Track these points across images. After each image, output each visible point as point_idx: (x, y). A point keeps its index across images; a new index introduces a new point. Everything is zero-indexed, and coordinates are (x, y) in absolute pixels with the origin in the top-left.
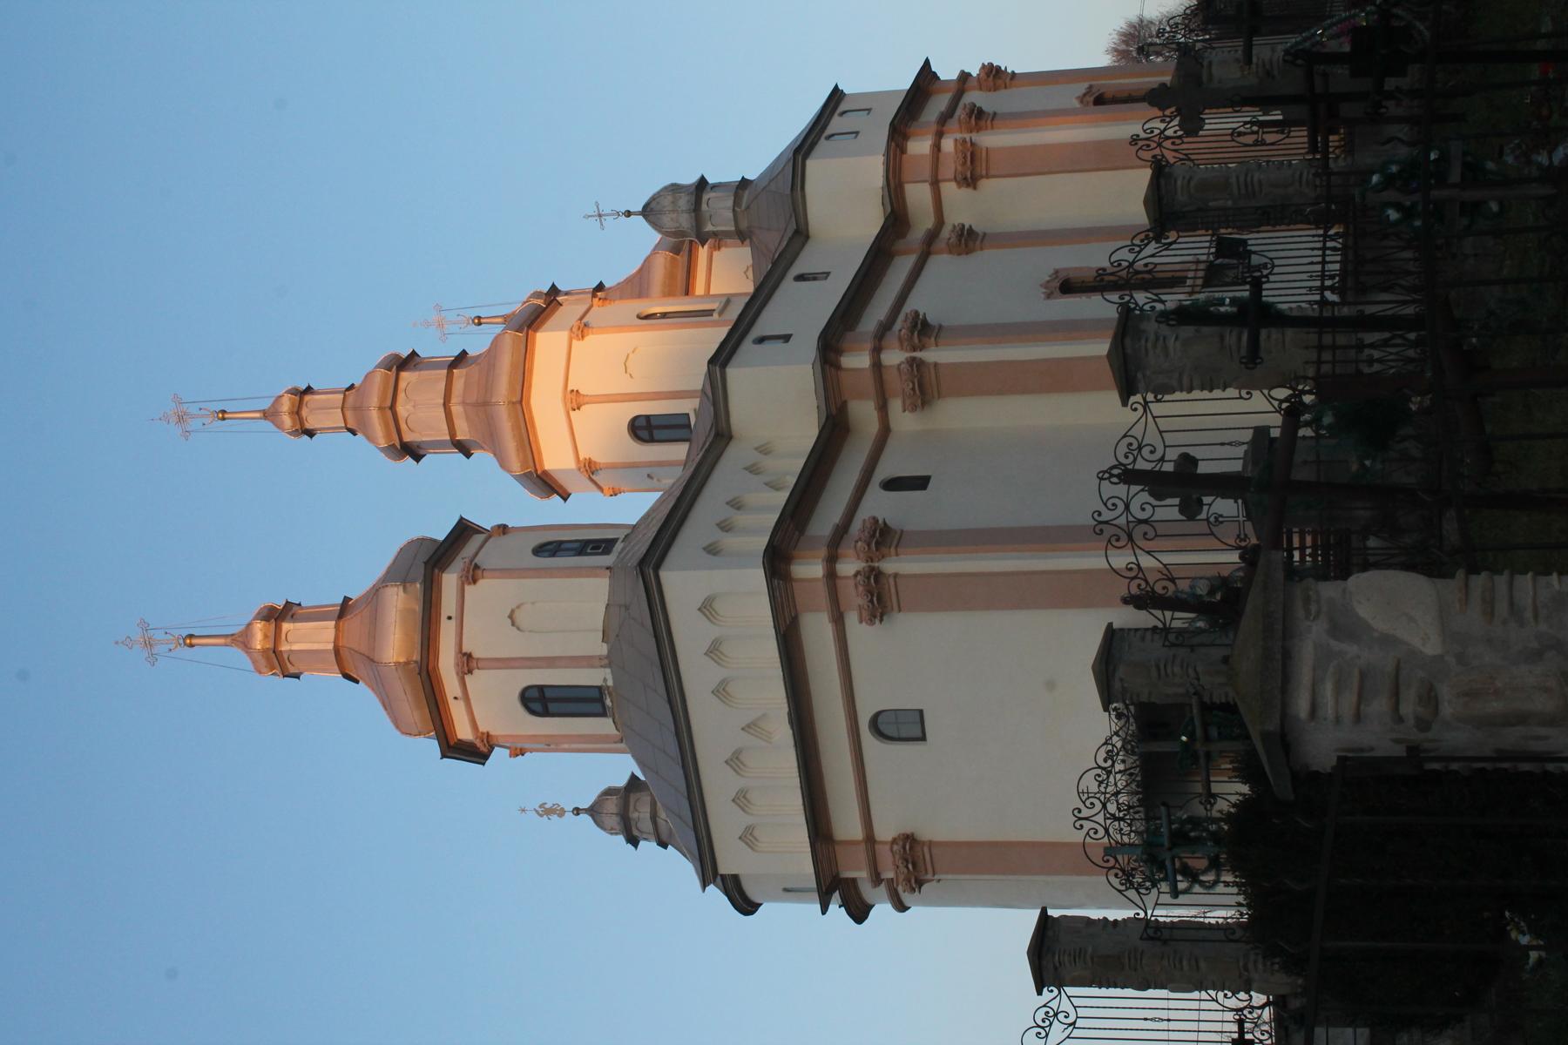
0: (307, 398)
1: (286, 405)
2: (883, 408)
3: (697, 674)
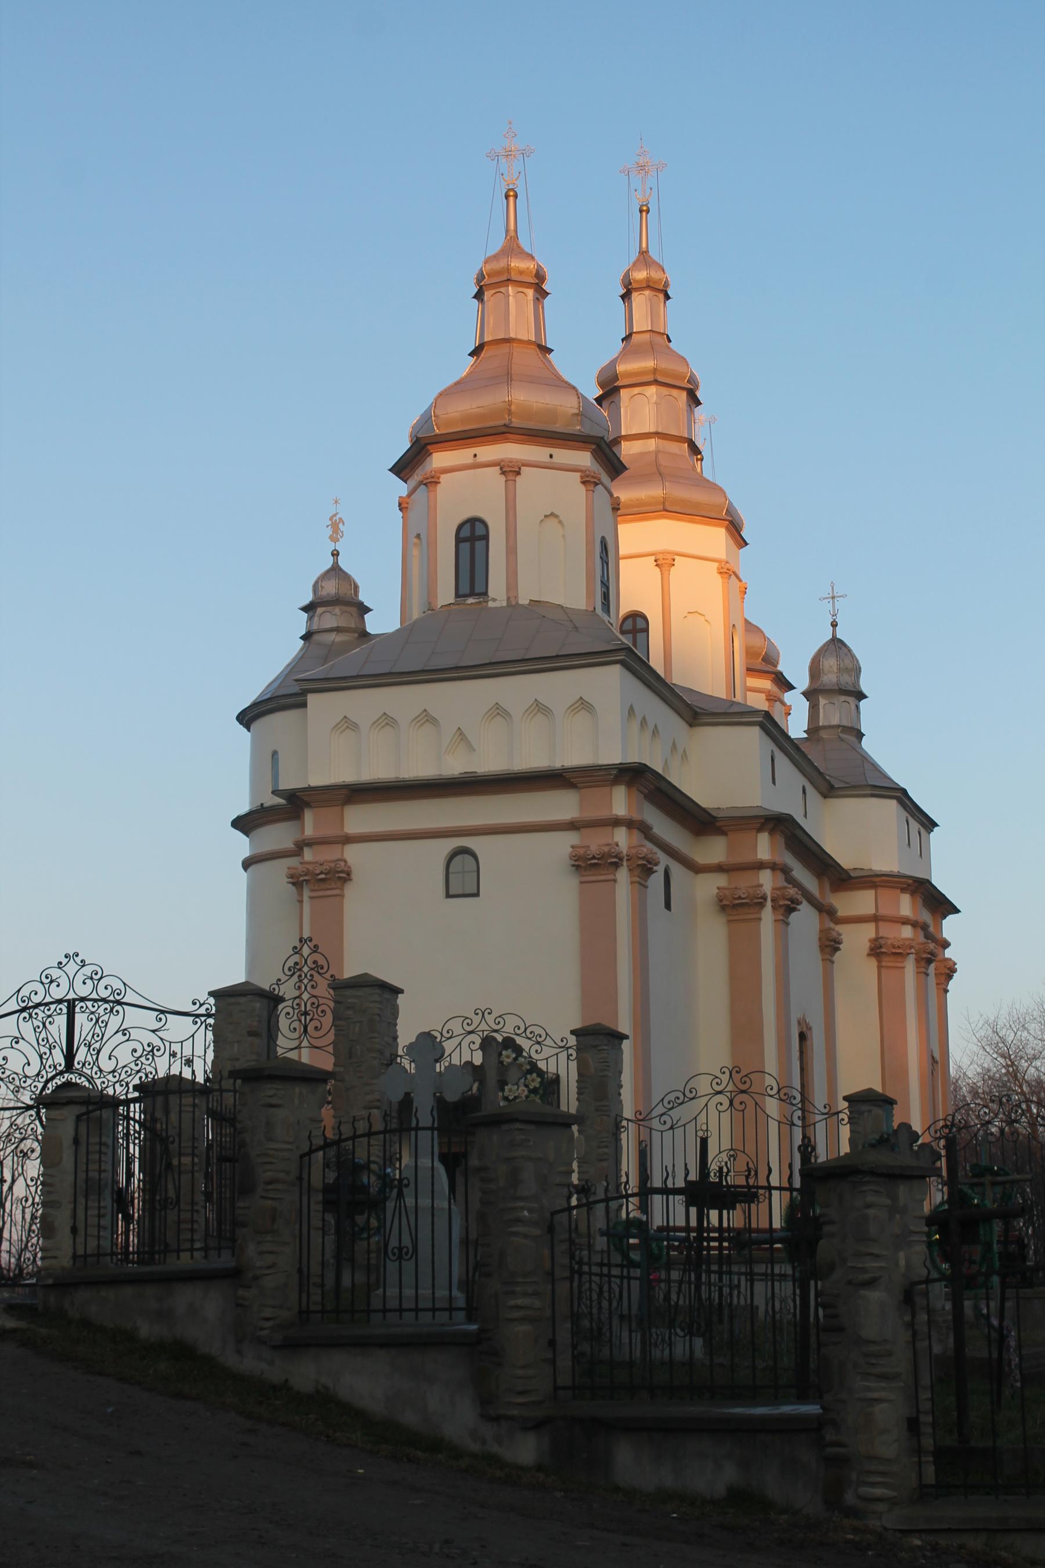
0: (661, 296)
1: (655, 275)
2: (719, 868)
3: (515, 690)
